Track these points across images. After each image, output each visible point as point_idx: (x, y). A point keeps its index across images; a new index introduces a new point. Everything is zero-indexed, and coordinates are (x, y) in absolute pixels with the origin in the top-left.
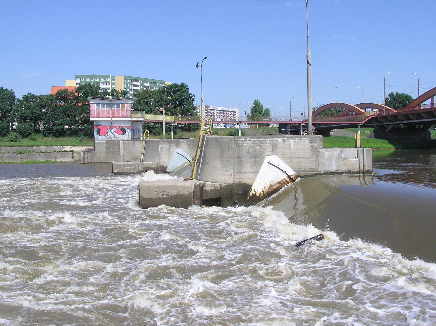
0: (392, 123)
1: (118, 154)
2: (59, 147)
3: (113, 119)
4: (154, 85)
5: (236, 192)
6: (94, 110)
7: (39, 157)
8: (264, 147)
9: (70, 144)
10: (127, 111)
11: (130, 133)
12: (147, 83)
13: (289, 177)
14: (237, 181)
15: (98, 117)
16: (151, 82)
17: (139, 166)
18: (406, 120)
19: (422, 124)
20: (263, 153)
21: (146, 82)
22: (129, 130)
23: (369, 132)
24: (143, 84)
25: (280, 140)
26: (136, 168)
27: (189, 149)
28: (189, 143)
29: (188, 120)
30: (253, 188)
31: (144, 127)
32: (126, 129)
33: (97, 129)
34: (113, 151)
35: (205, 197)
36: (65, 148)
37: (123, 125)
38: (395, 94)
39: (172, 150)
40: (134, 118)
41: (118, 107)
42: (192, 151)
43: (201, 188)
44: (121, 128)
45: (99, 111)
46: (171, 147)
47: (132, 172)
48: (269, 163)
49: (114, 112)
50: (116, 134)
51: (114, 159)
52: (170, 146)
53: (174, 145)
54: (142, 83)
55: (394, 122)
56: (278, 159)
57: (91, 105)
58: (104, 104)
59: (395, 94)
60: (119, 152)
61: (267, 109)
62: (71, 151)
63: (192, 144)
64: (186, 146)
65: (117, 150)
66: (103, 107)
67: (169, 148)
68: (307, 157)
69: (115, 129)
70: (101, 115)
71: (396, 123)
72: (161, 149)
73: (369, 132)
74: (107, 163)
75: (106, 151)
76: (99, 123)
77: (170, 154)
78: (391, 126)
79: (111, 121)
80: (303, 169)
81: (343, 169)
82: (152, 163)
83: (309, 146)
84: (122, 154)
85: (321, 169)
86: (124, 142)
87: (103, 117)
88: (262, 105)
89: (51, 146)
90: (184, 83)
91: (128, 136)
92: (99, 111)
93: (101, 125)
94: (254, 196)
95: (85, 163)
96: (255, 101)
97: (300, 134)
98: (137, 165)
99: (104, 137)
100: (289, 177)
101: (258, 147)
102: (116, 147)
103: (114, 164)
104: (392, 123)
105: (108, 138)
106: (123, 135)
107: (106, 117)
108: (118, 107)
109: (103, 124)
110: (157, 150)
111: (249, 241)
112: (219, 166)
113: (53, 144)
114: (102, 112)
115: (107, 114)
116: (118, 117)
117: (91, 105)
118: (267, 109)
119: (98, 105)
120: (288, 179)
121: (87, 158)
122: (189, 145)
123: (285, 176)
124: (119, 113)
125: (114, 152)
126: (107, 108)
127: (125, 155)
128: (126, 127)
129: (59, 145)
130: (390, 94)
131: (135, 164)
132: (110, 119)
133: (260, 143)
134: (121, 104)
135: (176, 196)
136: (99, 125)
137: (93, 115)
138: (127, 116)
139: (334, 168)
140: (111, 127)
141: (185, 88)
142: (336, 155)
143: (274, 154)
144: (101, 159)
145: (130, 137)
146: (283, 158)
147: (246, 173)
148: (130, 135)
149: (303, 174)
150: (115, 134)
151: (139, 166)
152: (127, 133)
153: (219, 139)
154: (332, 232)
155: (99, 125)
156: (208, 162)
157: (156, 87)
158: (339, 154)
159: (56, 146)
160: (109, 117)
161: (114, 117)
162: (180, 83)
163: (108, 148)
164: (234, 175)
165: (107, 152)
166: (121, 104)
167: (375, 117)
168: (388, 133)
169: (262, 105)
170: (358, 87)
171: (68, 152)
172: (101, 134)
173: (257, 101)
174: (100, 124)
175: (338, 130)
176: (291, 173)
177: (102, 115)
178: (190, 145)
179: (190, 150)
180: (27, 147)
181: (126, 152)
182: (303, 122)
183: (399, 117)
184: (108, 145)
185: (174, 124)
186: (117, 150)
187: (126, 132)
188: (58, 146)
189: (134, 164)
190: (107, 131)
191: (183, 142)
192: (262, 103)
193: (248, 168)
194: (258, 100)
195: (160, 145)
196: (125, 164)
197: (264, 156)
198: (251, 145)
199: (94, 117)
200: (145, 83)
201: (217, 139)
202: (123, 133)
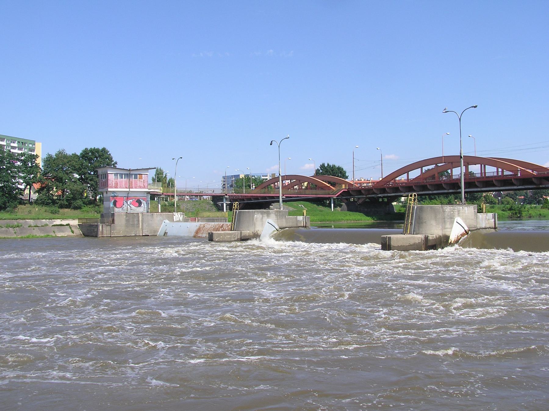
0: (364, 196)
2: (47, 220)
3: (131, 190)
4: (23, 146)
5: (443, 240)
6: (112, 180)
7: (34, 231)
8: (454, 212)
9: (59, 217)
10: (144, 182)
11: (146, 204)
12: (14, 143)
13: (465, 231)
14: (444, 233)
15: (116, 187)
16: (19, 142)
17: (238, 235)
18: (380, 194)
20: (454, 216)
21: (12, 141)
22: (144, 202)
23: (302, 206)
24: (10, 144)
25: (461, 208)
27: (277, 219)
28: (276, 214)
29: (28, 188)
30: (450, 238)
32: (142, 201)
33: (113, 201)
35: (430, 244)
36: (55, 221)
37: (139, 196)
38: (326, 165)
39: (264, 219)
40: (151, 189)
41: (136, 178)
42: (279, 220)
43: (426, 238)
44: (137, 199)
45: (116, 181)
46: (264, 217)
47: (232, 240)
48: (457, 222)
50: (132, 206)
51: (134, 232)
52: (262, 216)
53: (265, 215)
54: (8, 142)
55: (367, 195)
56: (461, 219)
57: (109, 174)
58: (122, 174)
59: (326, 165)
60: (138, 225)
61: (171, 178)
62: (67, 225)
63: (279, 215)
64: (274, 216)
65: (136, 223)
66: (120, 177)
67: (262, 218)
68: (472, 218)
69: (131, 201)
70: (119, 186)
71: (370, 196)
72: (256, 219)
73: (302, 206)
75: (126, 224)
76: (115, 195)
77: (262, 225)
78: (363, 200)
79: (128, 192)
80: (471, 226)
81: (488, 226)
82: (249, 232)
83: (473, 212)
85: (479, 227)
87: (121, 187)
89: (38, 219)
90: (105, 147)
91: (144, 208)
93: (117, 196)
94: (451, 243)
98: (237, 234)
99: (120, 209)
100: (465, 231)
101: (452, 212)
103: (215, 233)
104: (364, 196)
105: (125, 210)
106: (139, 208)
107: (123, 188)
108: (136, 178)
112: (434, 224)
113: (40, 218)
114: (120, 182)
115: (125, 184)
116: (136, 188)
117: (109, 174)
118: (171, 178)
119: (116, 175)
120: (465, 232)
121: (105, 232)
122: (276, 215)
123: (463, 231)
124: (136, 184)
125: (133, 225)
126: (124, 178)
128: (142, 199)
129: (47, 218)
130: (321, 165)
132: (128, 190)
133: (454, 209)
134: (139, 174)
135: (414, 244)
136: (115, 196)
137: (111, 186)
138: (144, 187)
139: (483, 226)
140: (128, 198)
141: (107, 153)
142: (484, 217)
143: (459, 217)
144: (121, 233)
146: (463, 219)
147: (447, 228)
148: (146, 207)
149: (471, 229)
150: (131, 205)
151: (238, 235)
152: (142, 205)
153: (433, 207)
155: (115, 196)
156: (426, 222)
157: (25, 149)
158: (486, 217)
159: (44, 219)
160: (126, 188)
161: (132, 188)
163: (127, 221)
164: (442, 230)
165: (127, 226)
166: (139, 174)
167: (347, 190)
168: (359, 206)
170: (311, 159)
171: (63, 225)
172: (117, 205)
173: (160, 169)
174: (117, 195)
176: (466, 229)
178: (277, 215)
179: (278, 220)
180: (11, 220)
181: (145, 225)
182: (226, 195)
183: (363, 192)
184: (128, 218)
186: (136, 223)
187: (142, 204)
190: (123, 203)
191: (272, 213)
193: (448, 226)
195: (255, 216)
197: (454, 217)
198: (449, 210)
199: (112, 188)
200: (11, 142)
201: (431, 207)
202: (139, 205)
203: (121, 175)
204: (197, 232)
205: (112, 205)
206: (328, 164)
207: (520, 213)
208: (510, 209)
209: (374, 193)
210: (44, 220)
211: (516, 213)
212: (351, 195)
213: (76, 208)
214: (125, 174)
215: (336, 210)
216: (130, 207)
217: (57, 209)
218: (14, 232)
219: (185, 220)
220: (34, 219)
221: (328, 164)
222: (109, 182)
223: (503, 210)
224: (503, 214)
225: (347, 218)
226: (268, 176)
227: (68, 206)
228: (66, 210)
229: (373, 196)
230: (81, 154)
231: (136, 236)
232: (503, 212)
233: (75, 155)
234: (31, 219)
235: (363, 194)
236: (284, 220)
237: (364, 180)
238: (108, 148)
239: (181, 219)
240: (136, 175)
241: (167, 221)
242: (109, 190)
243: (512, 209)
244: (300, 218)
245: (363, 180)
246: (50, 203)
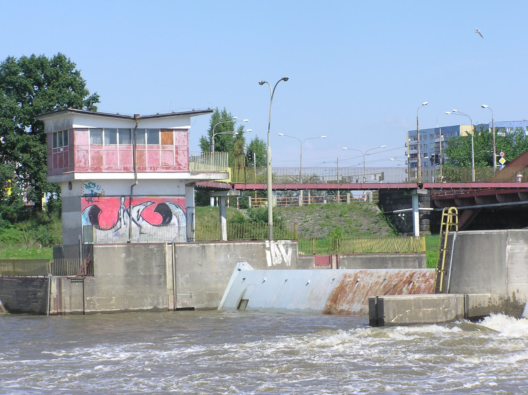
1: (159, 284)
3: (141, 176)
6: (84, 148)
10: (177, 153)
11: (183, 219)
15: (97, 169)
19: (450, 202)
26: (450, 311)
31: (240, 204)
32: (172, 207)
33: (88, 209)
34: (145, 276)
40: (198, 173)
49: (142, 154)
50: (144, 224)
51: (150, 301)
60: (162, 280)
69: (142, 207)
70: (105, 166)
72: (512, 256)
74: (134, 311)
75: (126, 276)
76: (95, 191)
79: (132, 184)
84: (169, 285)
86: (173, 244)
87: (110, 170)
92: (98, 152)
95: (61, 314)
97: (413, 235)
99: (110, 233)
102: (154, 263)
103: (388, 301)
106: (164, 228)
108: (153, 140)
109: (108, 191)
110: (501, 260)
116: (154, 170)
117: (76, 132)
119: (96, 132)
121: (68, 298)
125: (148, 279)
126: (121, 143)
127: (180, 286)
131: (449, 299)
132: (130, 176)
137: (82, 164)
138: (178, 168)
140: (131, 201)
144: (113, 302)
145: (183, 232)
152: (174, 220)
161: (143, 170)
162: (50, 56)
163: (131, 267)
166: (163, 130)
173: (224, 115)
174: (99, 192)
177: (108, 163)
181: (181, 280)
184: (132, 259)
185: (233, 193)
189: (443, 300)
190: (119, 214)
194: (228, 112)
195: (509, 247)
196: (419, 299)
199: (84, 170)
204: (335, 298)
205: (85, 222)
214: (121, 131)
222: (78, 155)
238: (71, 56)
239: (288, 258)
241: (246, 267)
242: (78, 176)
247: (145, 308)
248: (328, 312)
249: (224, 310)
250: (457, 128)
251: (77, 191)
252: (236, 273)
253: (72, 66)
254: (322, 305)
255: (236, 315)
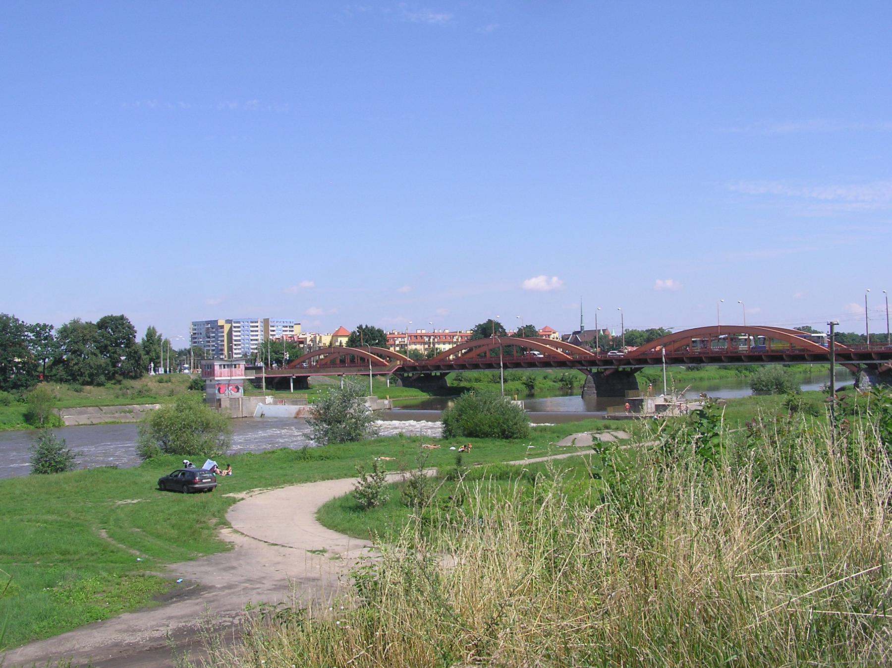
3: (233, 378)
15: (221, 376)
32: (239, 387)
50: (232, 392)
79: (230, 380)
87: (224, 376)
88: (151, 334)
96: (149, 329)
111: (705, 396)
116: (235, 376)
123: (236, 525)
124: (235, 373)
132: (229, 378)
138: (242, 375)
152: (240, 391)
154: (860, 335)
169: (151, 334)
172: (221, 392)
175: (192, 494)
188: (149, 404)
192: (157, 329)
199: (217, 377)
203: (224, 365)
204: (298, 414)
205: (217, 392)
206: (366, 326)
207: (571, 383)
208: (562, 380)
209: (429, 370)
210: (147, 405)
211: (567, 384)
212: (405, 371)
213: (99, 385)
214: (227, 365)
215: (376, 379)
216: (232, 393)
217: (79, 387)
218: (131, 417)
219: (275, 403)
220: (139, 404)
221: (366, 326)
222: (216, 372)
223: (555, 382)
224: (553, 385)
225: (405, 394)
226: (259, 322)
227: (90, 383)
228: (88, 387)
229: (428, 372)
230: (98, 323)
231: (237, 418)
232: (554, 384)
233: (90, 324)
234: (137, 404)
235: (418, 370)
236: (375, 404)
237: (398, 333)
238: (126, 315)
239: (272, 401)
240: (235, 365)
241: (261, 404)
242: (216, 379)
243: (564, 381)
244: (386, 402)
245: (396, 334)
246: (70, 380)
247: (91, 408)
248: (296, 418)
249: (256, 417)
250: (217, 321)
251: (213, 382)
252: (258, 406)
253: (128, 319)
254: (294, 415)
255: (260, 419)
